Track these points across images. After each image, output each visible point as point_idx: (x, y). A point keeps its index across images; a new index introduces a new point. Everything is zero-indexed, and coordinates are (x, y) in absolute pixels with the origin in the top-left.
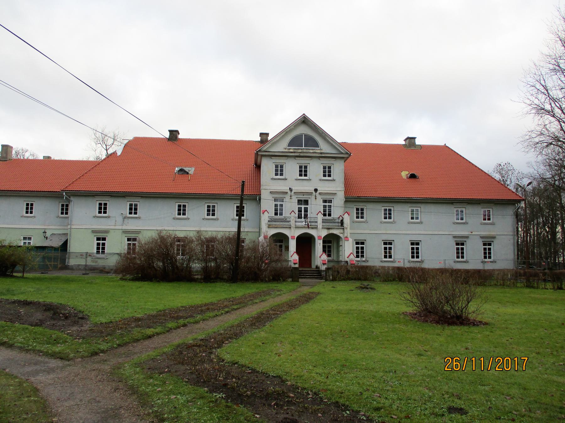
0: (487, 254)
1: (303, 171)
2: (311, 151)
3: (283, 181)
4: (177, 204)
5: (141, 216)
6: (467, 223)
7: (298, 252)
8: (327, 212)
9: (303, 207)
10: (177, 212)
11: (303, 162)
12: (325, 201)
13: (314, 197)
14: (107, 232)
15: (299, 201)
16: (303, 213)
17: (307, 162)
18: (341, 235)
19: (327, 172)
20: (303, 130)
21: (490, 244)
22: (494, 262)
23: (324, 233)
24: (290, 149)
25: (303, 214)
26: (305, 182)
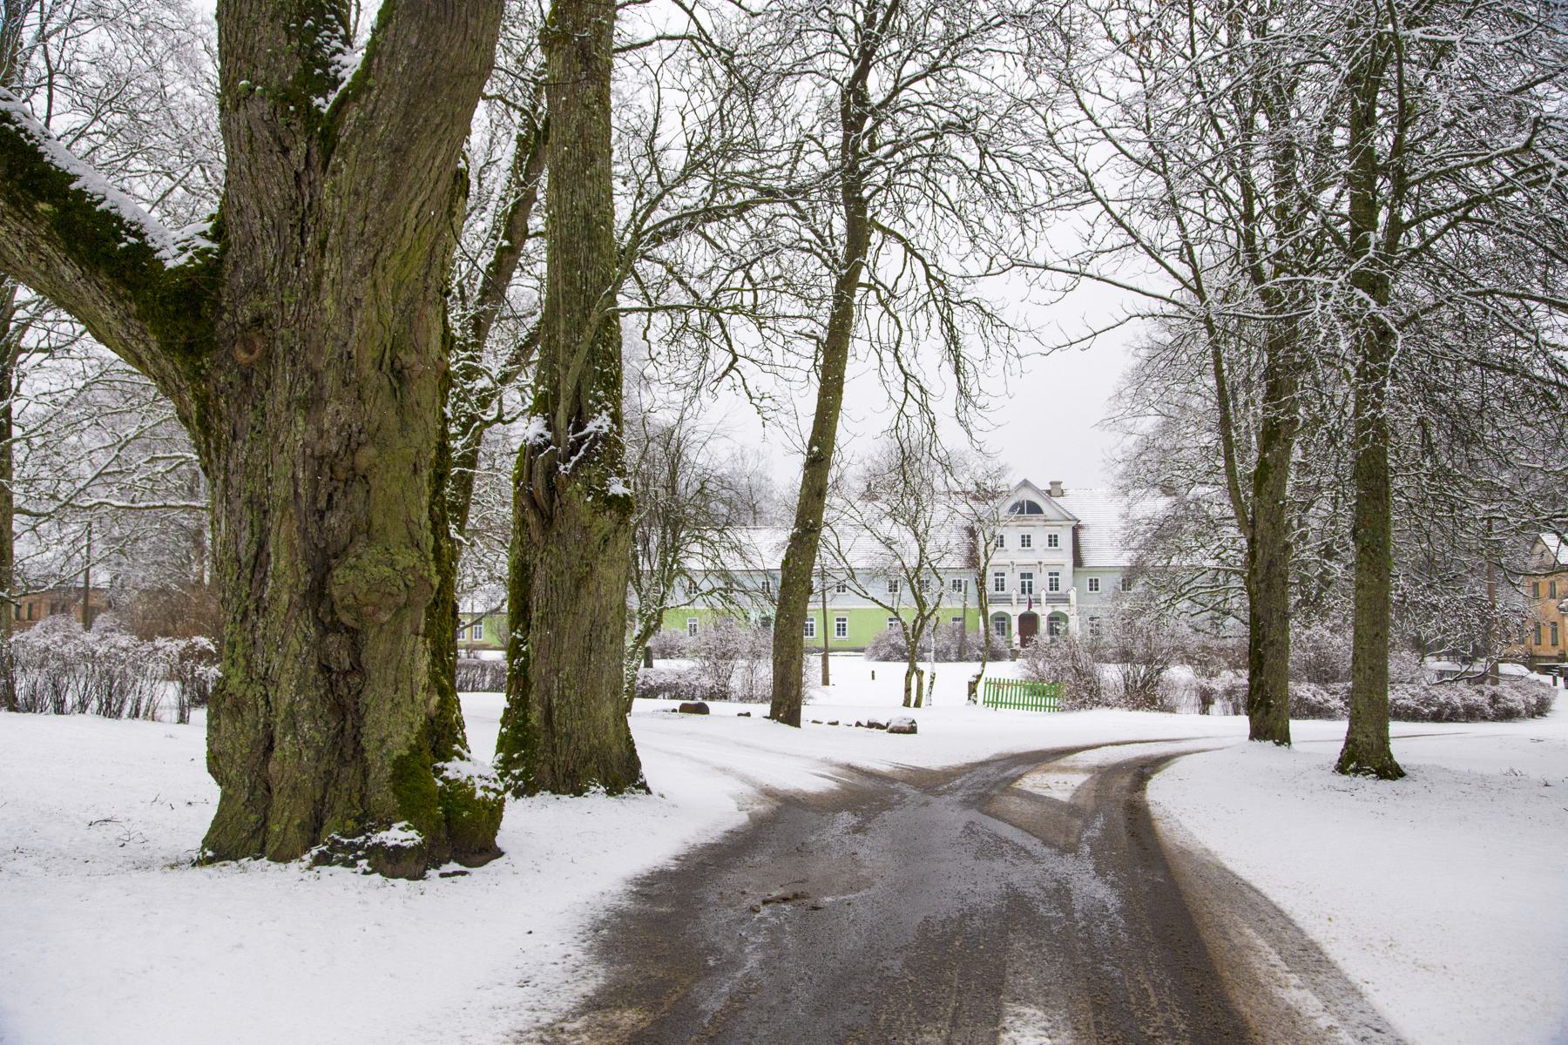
1: (1026, 541)
8: (1054, 585)
25: (1026, 588)
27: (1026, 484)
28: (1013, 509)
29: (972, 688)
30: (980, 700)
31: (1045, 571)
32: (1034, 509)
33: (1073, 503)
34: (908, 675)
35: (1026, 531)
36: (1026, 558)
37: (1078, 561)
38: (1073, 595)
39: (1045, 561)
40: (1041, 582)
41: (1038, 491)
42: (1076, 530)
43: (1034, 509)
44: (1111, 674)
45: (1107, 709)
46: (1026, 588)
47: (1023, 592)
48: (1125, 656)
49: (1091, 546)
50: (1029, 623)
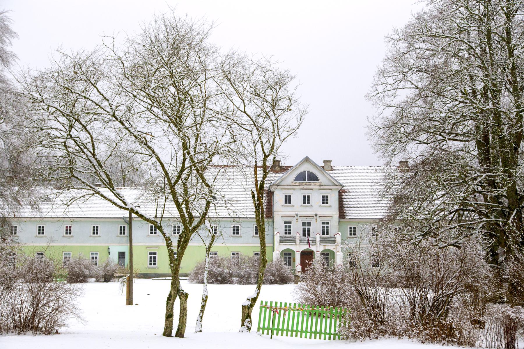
1: (306, 200)
7: (489, 138)
8: (325, 231)
9: (306, 227)
13: (315, 220)
15: (303, 223)
16: (306, 232)
18: (334, 251)
25: (306, 233)
27: (307, 160)
28: (297, 179)
29: (246, 314)
30: (254, 326)
31: (320, 221)
32: (313, 178)
33: (340, 175)
34: (170, 299)
35: (307, 193)
36: (307, 211)
37: (342, 215)
38: (338, 238)
39: (319, 214)
40: (316, 228)
41: (315, 166)
42: (341, 193)
43: (313, 178)
44: (396, 299)
45: (394, 340)
46: (306, 233)
47: (304, 235)
48: (411, 280)
49: (351, 204)
50: (307, 256)
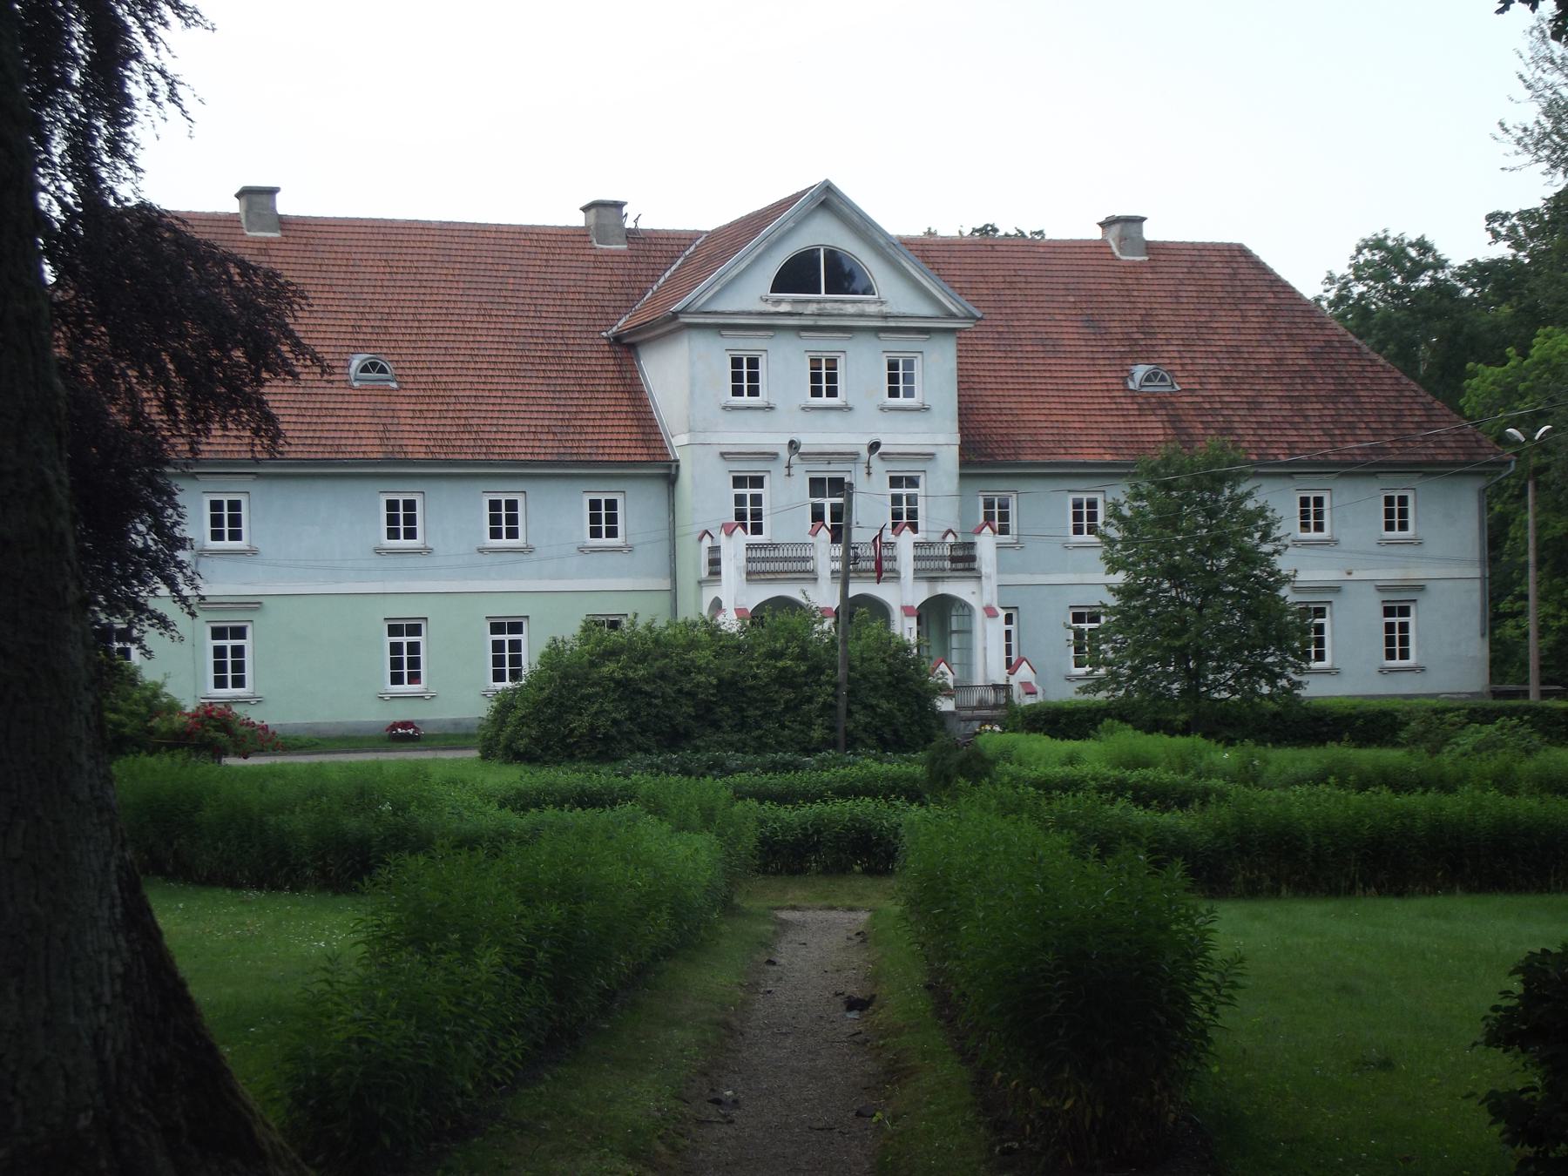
0: (1396, 642)
1: (824, 379)
2: (850, 309)
3: (760, 413)
4: (384, 499)
5: (256, 544)
6: (1336, 542)
10: (384, 527)
11: (824, 345)
12: (895, 482)
13: (862, 468)
14: (253, 605)
17: (838, 345)
19: (898, 378)
20: (822, 234)
21: (1405, 612)
22: (1418, 669)
23: (918, 594)
24: (779, 302)
26: (833, 417)
